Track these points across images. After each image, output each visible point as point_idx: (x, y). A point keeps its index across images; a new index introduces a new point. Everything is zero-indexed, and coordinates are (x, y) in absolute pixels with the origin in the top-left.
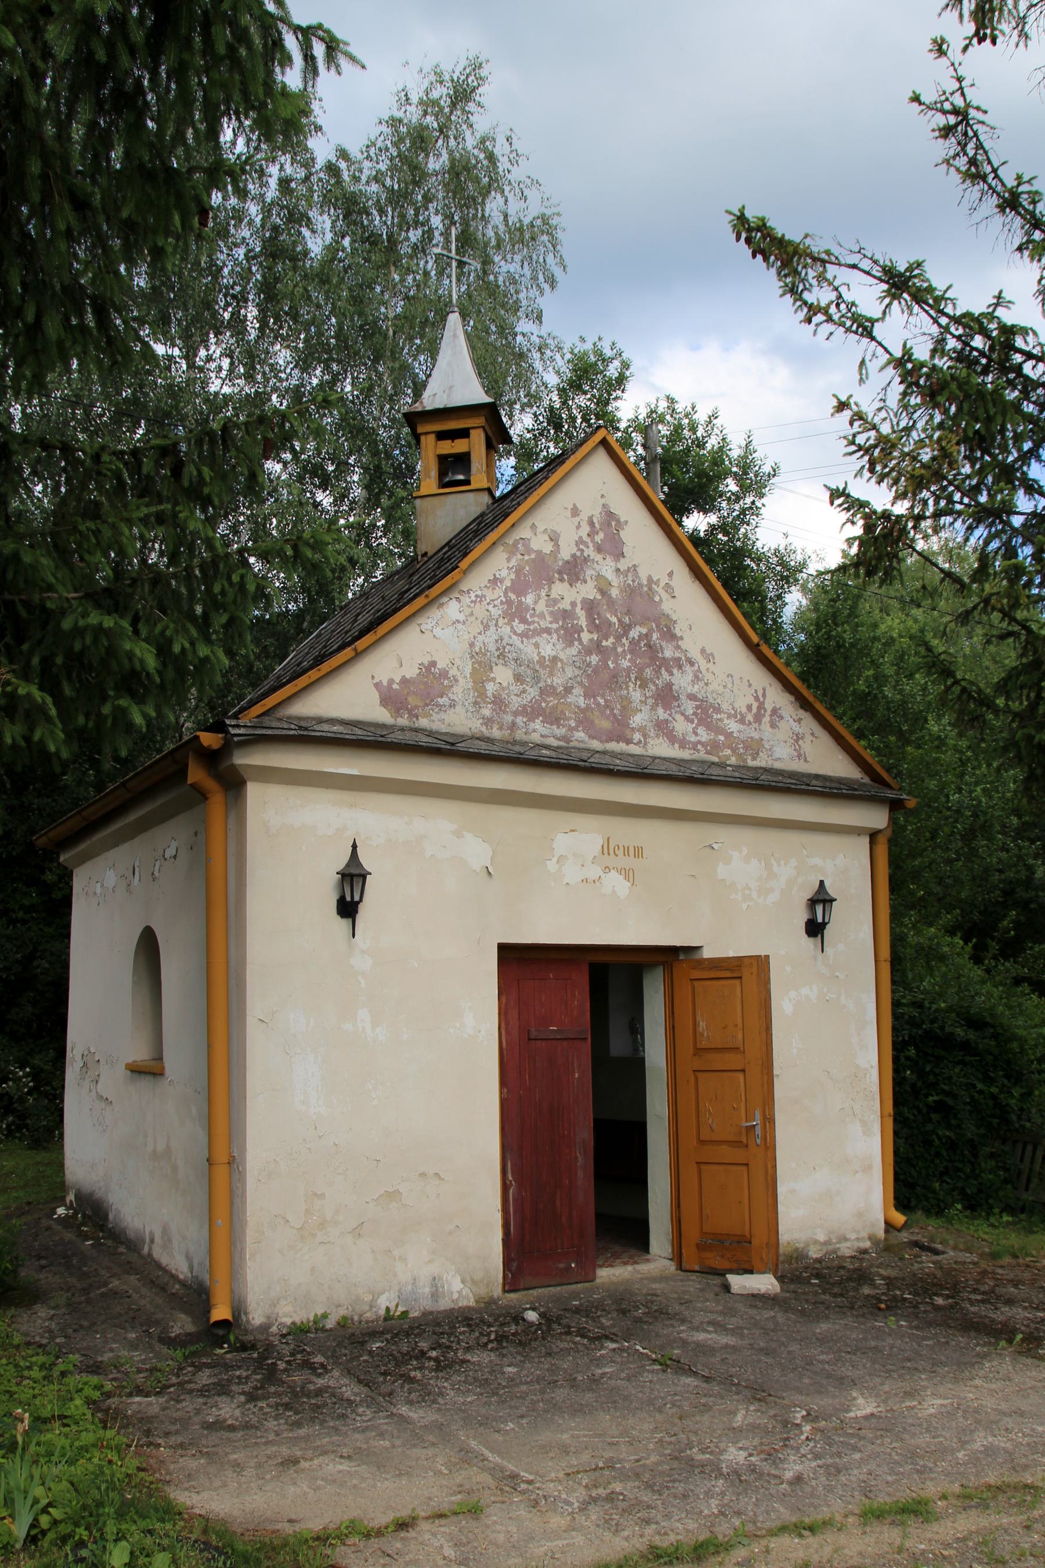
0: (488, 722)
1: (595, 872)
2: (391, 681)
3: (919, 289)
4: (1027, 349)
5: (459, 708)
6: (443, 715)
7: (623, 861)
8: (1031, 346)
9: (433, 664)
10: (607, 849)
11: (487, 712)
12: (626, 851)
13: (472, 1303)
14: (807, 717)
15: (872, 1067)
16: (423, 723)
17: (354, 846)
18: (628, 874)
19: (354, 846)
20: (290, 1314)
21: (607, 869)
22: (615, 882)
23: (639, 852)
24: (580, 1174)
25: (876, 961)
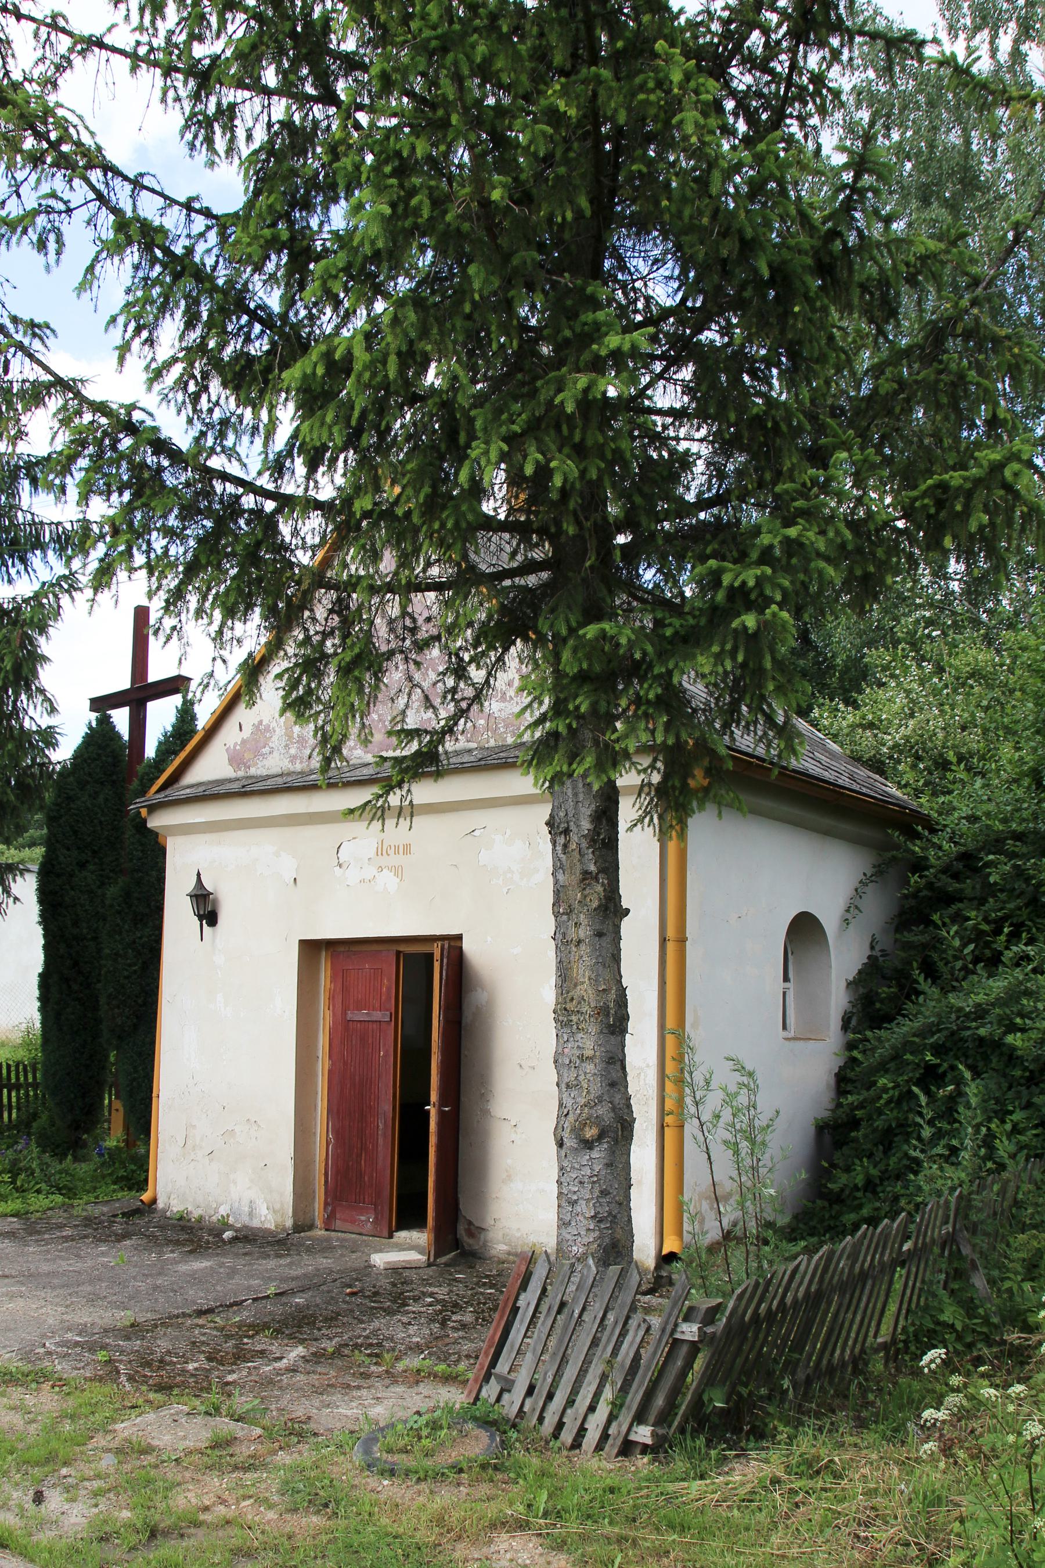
0: (293, 759)
1: (370, 871)
2: (236, 744)
3: (328, 372)
4: (248, 479)
5: (276, 754)
6: (265, 762)
7: (394, 860)
8: (253, 474)
9: (261, 722)
10: (381, 851)
11: (293, 751)
12: (397, 851)
13: (273, 1227)
14: (279, 771)
15: (648, 1066)
16: (253, 771)
17: (199, 875)
18: (397, 871)
19: (199, 875)
20: (176, 1207)
21: (381, 869)
22: (388, 880)
23: (407, 849)
24: (381, 1141)
25: (663, 941)
